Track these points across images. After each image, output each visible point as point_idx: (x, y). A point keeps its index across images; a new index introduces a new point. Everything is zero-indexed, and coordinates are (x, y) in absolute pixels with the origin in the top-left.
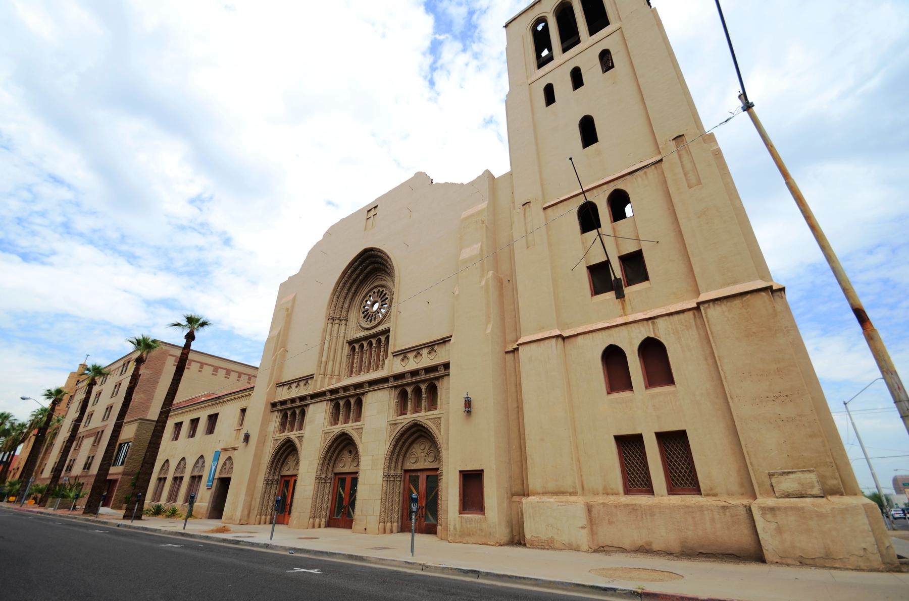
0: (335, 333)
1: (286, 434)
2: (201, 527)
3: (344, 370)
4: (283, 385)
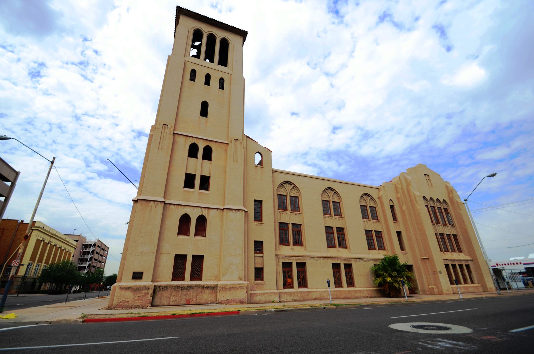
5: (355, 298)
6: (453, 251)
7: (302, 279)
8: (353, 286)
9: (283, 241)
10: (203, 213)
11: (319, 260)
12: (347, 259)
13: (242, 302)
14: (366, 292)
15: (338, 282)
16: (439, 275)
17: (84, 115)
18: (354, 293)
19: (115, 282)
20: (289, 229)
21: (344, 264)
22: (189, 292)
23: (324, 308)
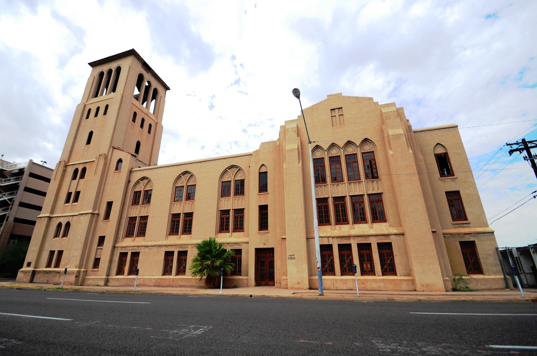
5: (179, 286)
7: (348, 265)
8: (395, 274)
9: (324, 220)
11: (143, 248)
12: (183, 246)
13: (71, 284)
14: (194, 280)
15: (349, 269)
16: (288, 261)
17: (248, 126)
18: (179, 282)
19: (22, 268)
20: (128, 223)
21: (378, 244)
22: (49, 275)
23: (251, 296)
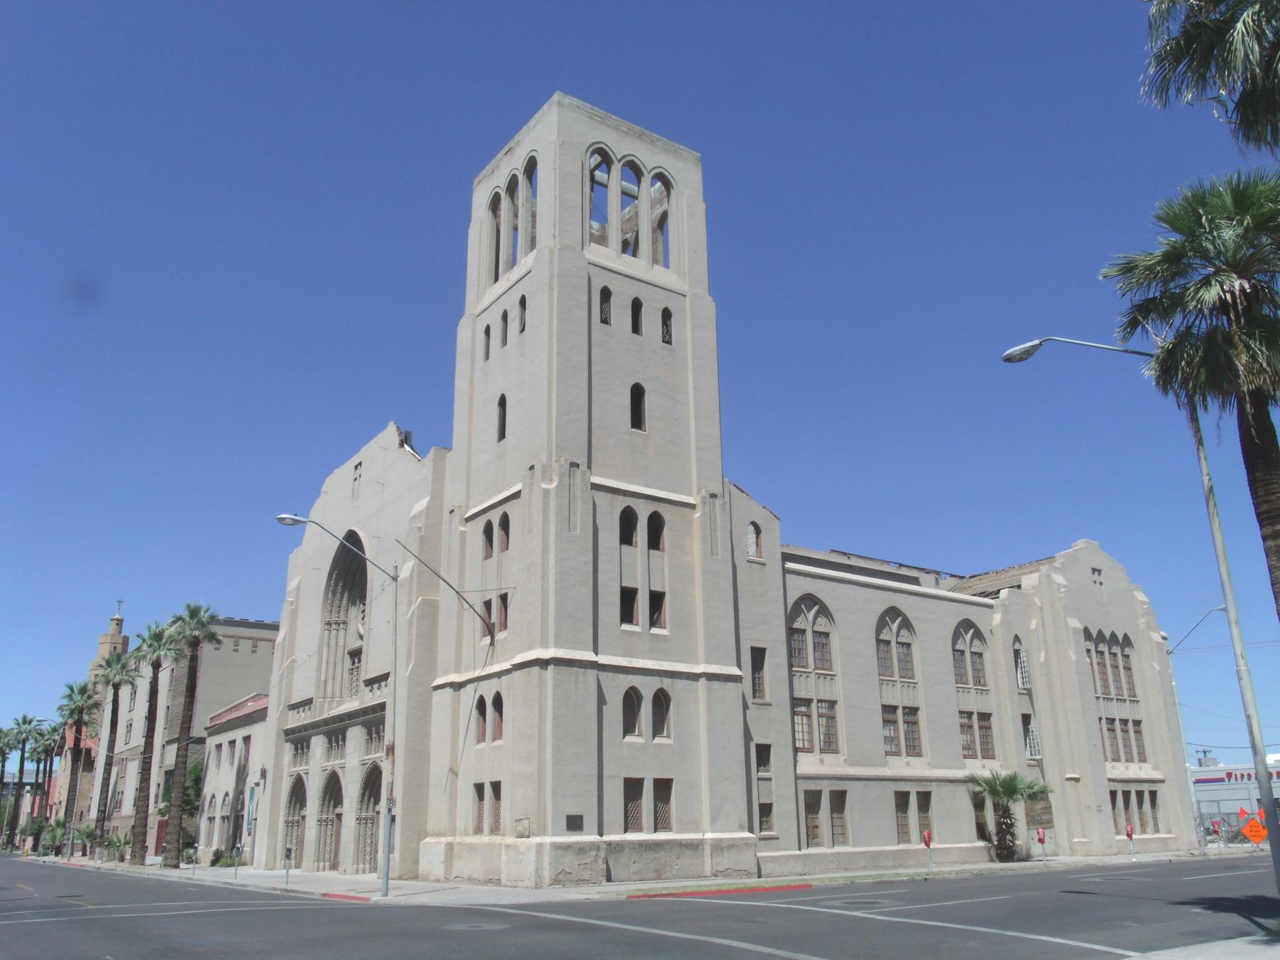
0: (333, 643)
1: (298, 769)
2: (201, 873)
3: (982, 581)
4: (294, 707)
6: (1129, 759)
10: (662, 684)
